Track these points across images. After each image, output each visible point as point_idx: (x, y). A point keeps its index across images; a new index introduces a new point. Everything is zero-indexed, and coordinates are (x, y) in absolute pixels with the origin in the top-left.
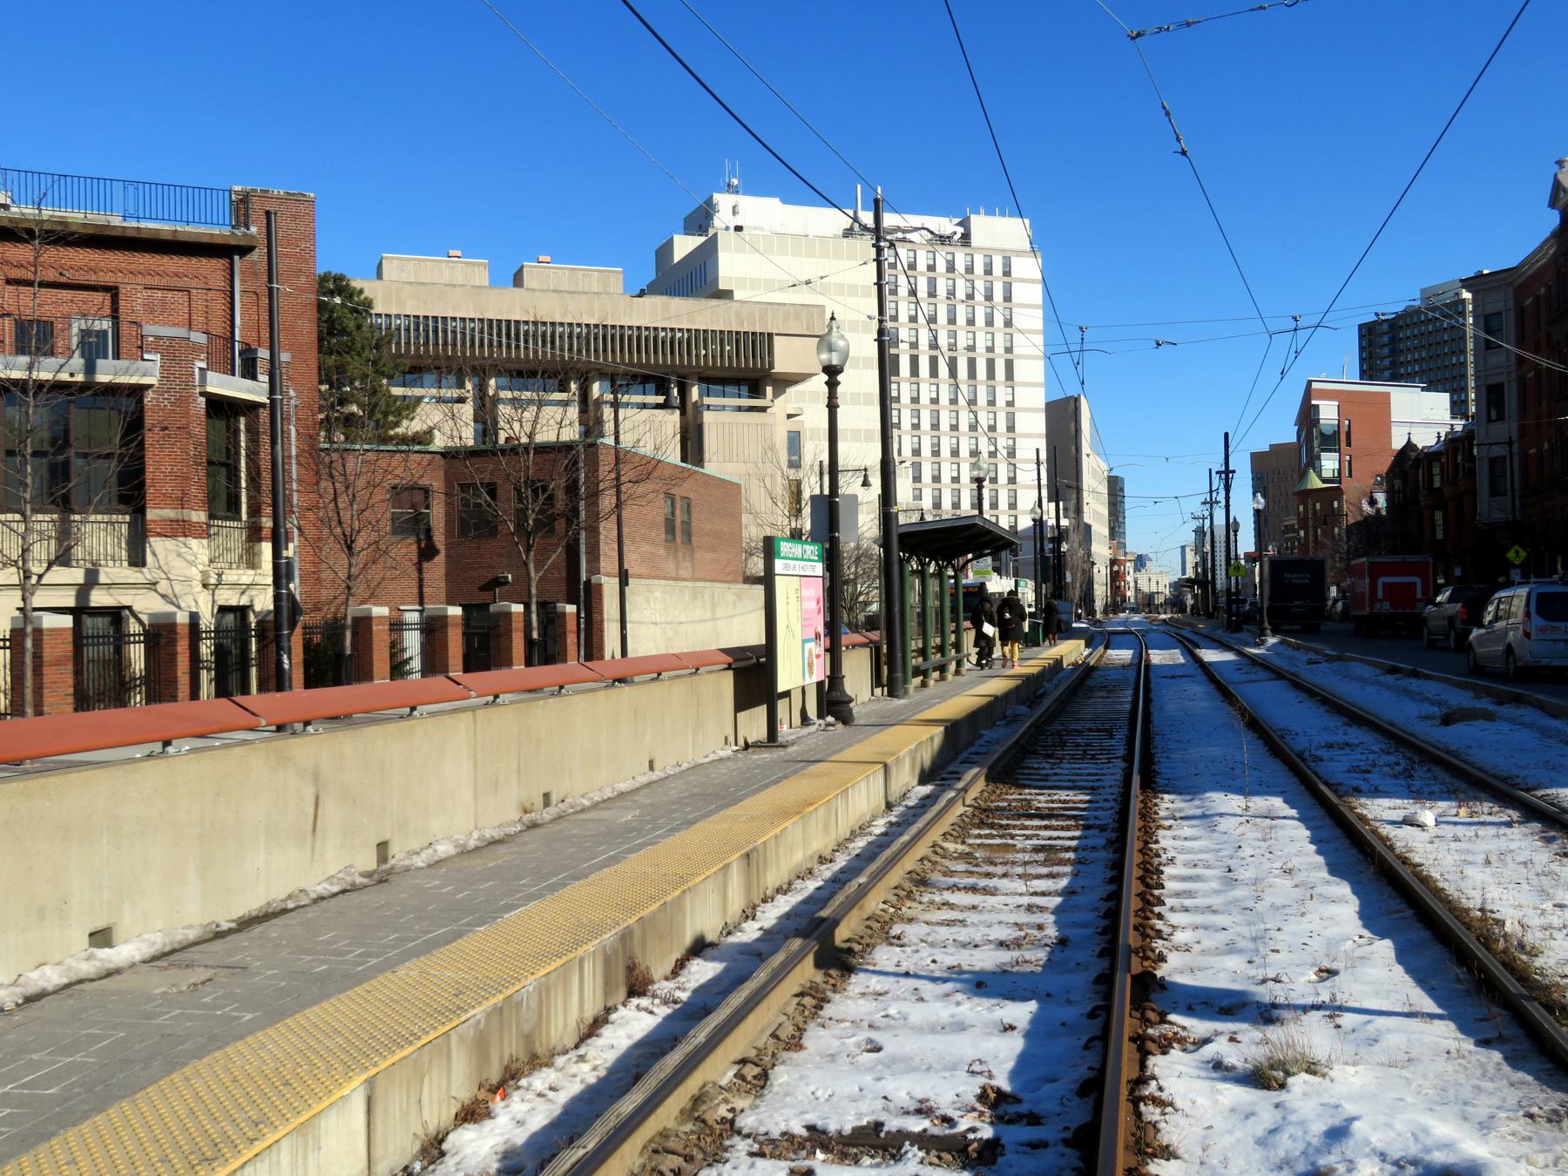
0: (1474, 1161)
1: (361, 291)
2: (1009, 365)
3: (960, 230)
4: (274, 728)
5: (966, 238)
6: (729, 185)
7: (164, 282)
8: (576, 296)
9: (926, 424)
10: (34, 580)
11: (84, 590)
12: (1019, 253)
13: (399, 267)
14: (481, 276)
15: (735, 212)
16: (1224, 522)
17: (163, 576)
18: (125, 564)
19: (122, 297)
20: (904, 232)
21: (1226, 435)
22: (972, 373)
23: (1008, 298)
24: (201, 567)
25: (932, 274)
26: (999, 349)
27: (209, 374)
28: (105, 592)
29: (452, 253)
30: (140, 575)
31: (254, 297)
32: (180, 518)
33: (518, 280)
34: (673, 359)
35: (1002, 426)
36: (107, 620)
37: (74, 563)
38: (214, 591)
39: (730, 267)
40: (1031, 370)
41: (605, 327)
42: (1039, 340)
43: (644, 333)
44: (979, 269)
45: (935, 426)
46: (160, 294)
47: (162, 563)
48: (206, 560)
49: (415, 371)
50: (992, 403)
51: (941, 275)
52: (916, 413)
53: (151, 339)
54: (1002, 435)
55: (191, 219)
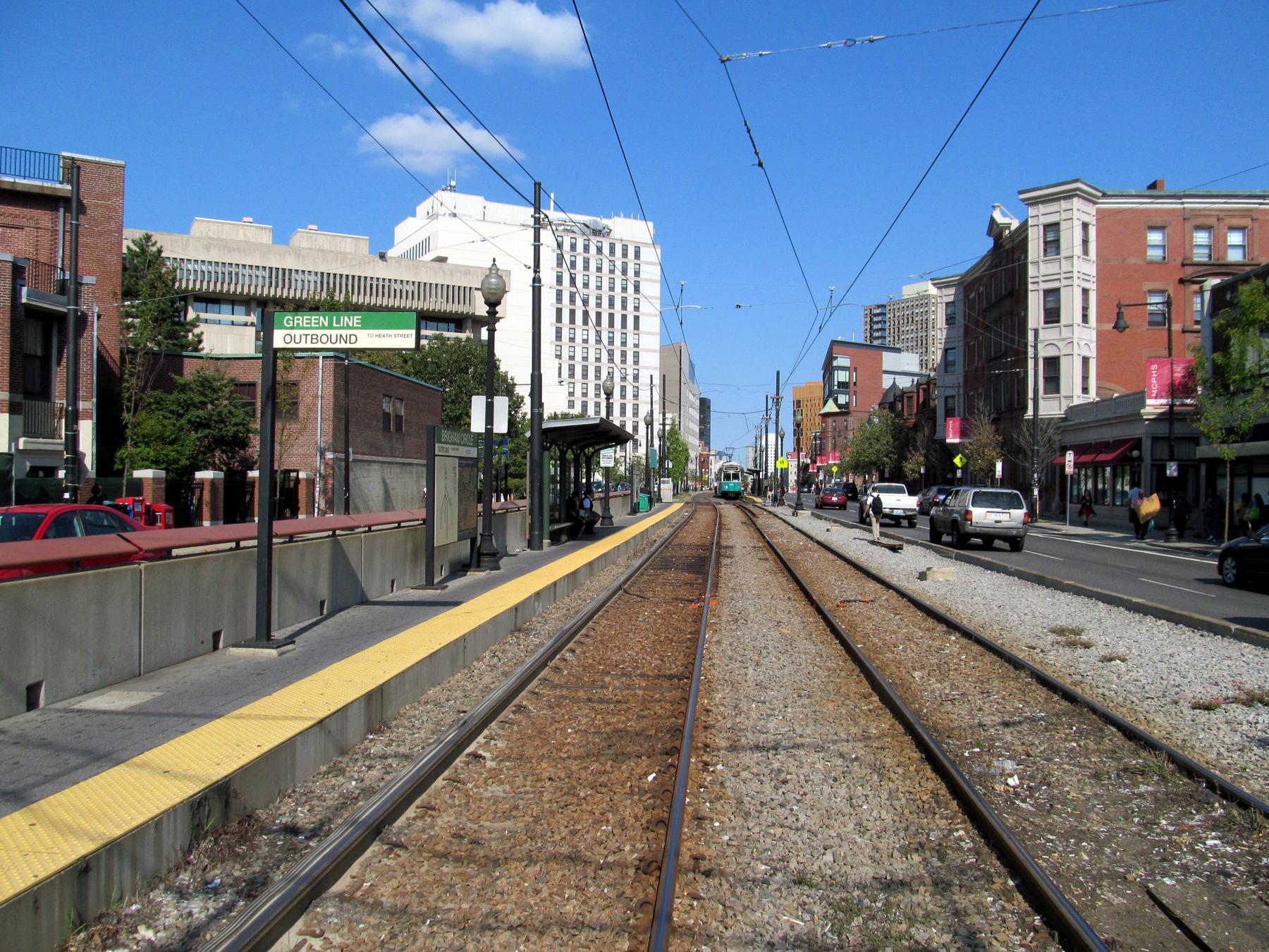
4: (175, 552)
13: (204, 227)
16: (769, 435)
21: (778, 373)
42: (657, 304)
43: (381, 283)
49: (211, 300)
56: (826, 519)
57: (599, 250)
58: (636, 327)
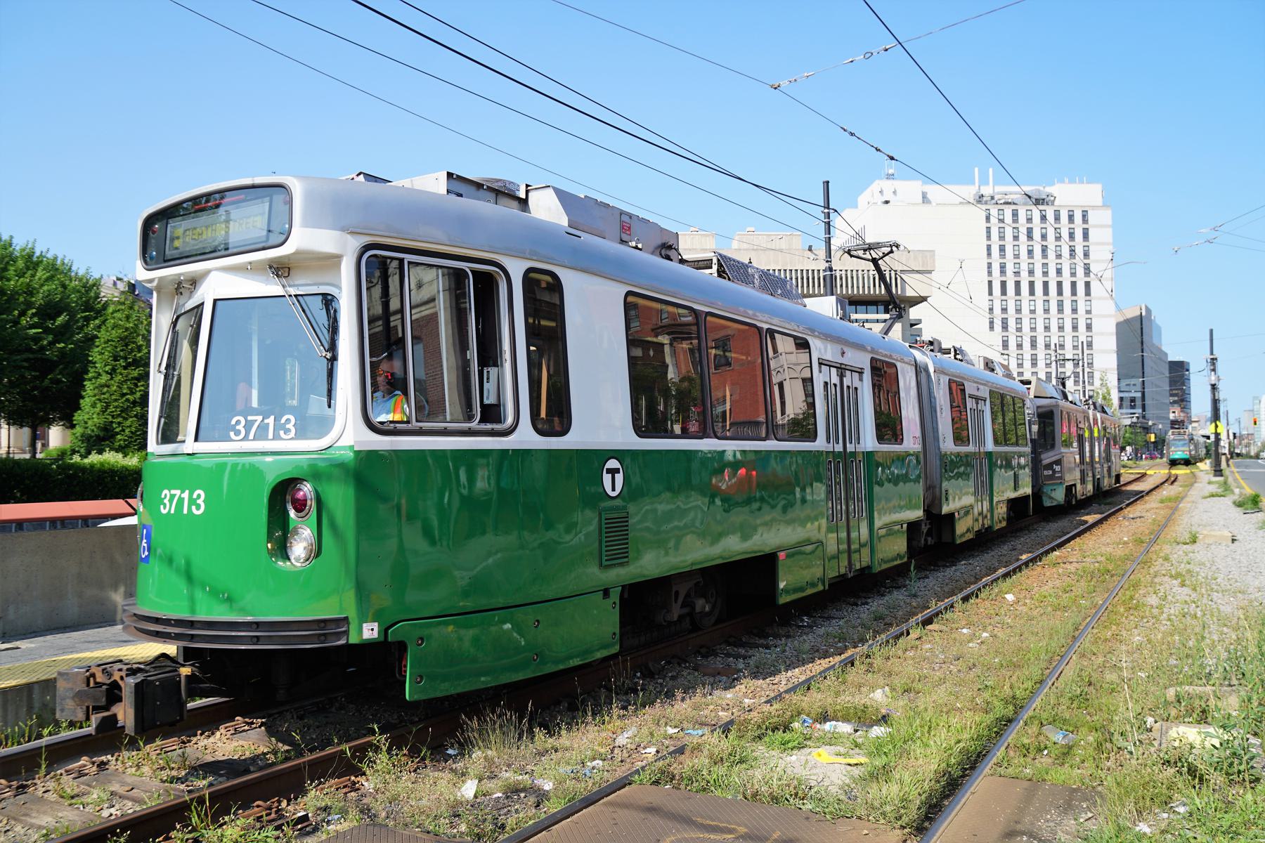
21: (1211, 331)
57: (1044, 218)
58: (1088, 293)
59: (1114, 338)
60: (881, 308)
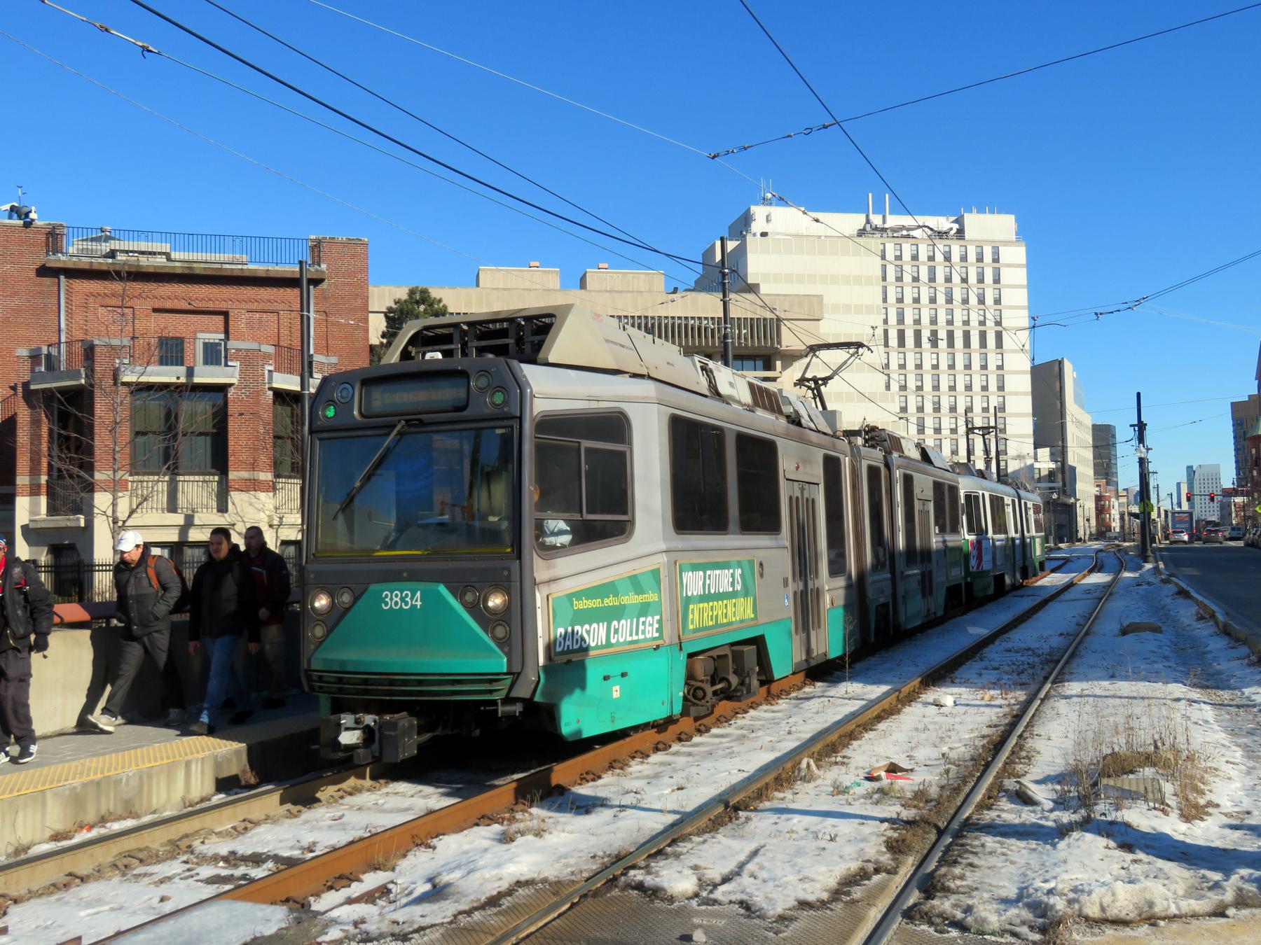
0: (310, 808)
1: (440, 301)
2: (999, 336)
3: (956, 226)
5: (960, 233)
6: (764, 199)
7: (261, 307)
8: (624, 294)
9: (928, 386)
10: (120, 524)
11: (184, 529)
12: (1007, 243)
14: (554, 281)
15: (768, 219)
17: (239, 519)
18: (215, 510)
19: (231, 318)
20: (908, 229)
21: (1139, 395)
22: (967, 344)
23: (997, 280)
24: (268, 513)
25: (931, 263)
26: (974, 322)
27: (275, 374)
28: (199, 530)
29: (532, 264)
30: (223, 519)
31: (324, 315)
32: (252, 477)
33: (583, 284)
34: (700, 342)
35: (993, 386)
36: (202, 550)
37: (179, 511)
38: (277, 530)
39: (757, 265)
40: (1016, 340)
41: (646, 317)
44: (972, 257)
45: (936, 388)
46: (258, 315)
47: (239, 510)
48: (272, 507)
50: (984, 367)
51: (940, 264)
52: (919, 377)
53: (233, 351)
54: (993, 393)
55: (279, 261)
56: (33, 895)
59: (1029, 399)
60: (760, 363)
